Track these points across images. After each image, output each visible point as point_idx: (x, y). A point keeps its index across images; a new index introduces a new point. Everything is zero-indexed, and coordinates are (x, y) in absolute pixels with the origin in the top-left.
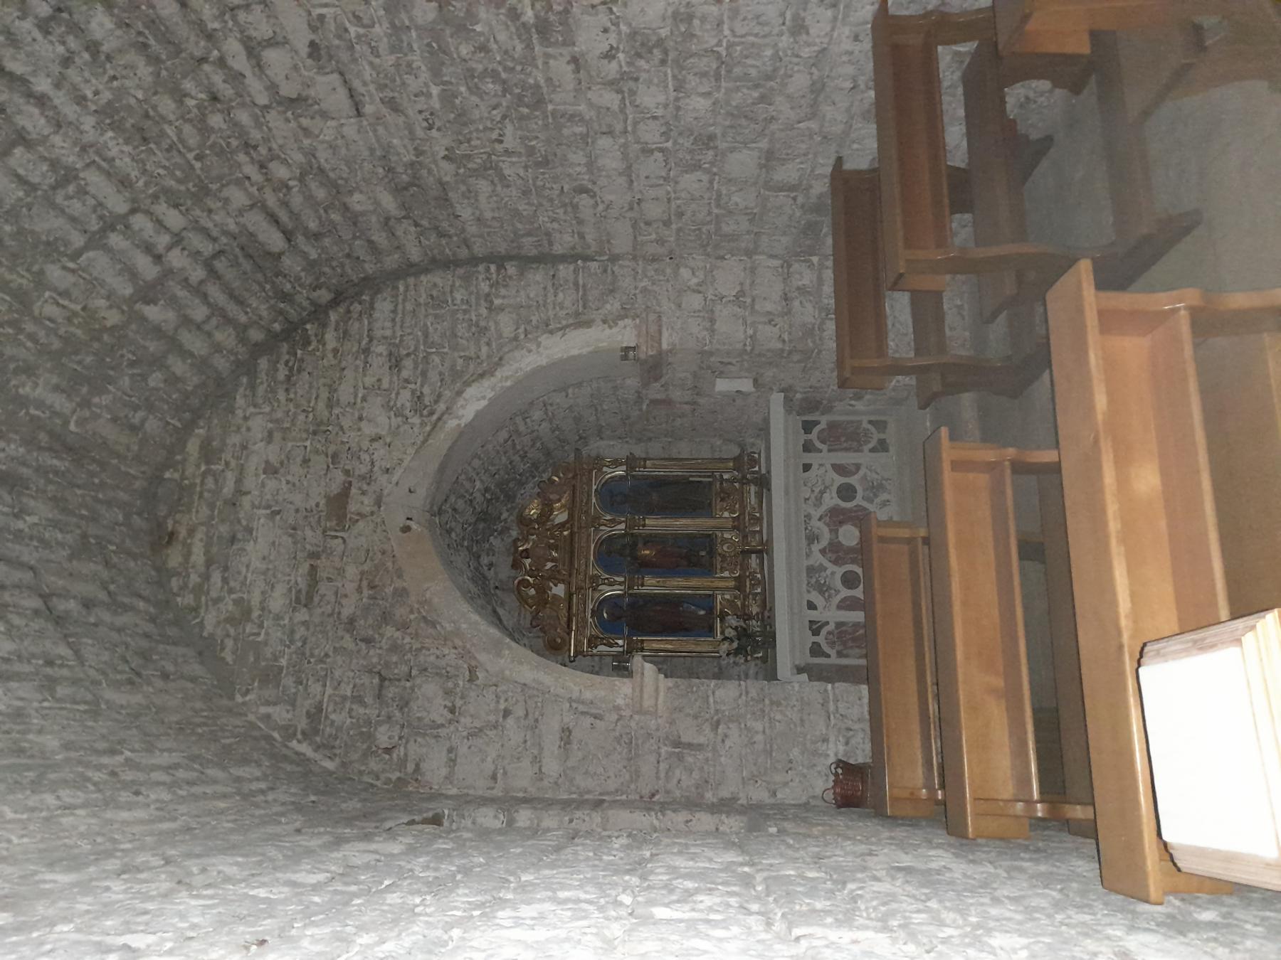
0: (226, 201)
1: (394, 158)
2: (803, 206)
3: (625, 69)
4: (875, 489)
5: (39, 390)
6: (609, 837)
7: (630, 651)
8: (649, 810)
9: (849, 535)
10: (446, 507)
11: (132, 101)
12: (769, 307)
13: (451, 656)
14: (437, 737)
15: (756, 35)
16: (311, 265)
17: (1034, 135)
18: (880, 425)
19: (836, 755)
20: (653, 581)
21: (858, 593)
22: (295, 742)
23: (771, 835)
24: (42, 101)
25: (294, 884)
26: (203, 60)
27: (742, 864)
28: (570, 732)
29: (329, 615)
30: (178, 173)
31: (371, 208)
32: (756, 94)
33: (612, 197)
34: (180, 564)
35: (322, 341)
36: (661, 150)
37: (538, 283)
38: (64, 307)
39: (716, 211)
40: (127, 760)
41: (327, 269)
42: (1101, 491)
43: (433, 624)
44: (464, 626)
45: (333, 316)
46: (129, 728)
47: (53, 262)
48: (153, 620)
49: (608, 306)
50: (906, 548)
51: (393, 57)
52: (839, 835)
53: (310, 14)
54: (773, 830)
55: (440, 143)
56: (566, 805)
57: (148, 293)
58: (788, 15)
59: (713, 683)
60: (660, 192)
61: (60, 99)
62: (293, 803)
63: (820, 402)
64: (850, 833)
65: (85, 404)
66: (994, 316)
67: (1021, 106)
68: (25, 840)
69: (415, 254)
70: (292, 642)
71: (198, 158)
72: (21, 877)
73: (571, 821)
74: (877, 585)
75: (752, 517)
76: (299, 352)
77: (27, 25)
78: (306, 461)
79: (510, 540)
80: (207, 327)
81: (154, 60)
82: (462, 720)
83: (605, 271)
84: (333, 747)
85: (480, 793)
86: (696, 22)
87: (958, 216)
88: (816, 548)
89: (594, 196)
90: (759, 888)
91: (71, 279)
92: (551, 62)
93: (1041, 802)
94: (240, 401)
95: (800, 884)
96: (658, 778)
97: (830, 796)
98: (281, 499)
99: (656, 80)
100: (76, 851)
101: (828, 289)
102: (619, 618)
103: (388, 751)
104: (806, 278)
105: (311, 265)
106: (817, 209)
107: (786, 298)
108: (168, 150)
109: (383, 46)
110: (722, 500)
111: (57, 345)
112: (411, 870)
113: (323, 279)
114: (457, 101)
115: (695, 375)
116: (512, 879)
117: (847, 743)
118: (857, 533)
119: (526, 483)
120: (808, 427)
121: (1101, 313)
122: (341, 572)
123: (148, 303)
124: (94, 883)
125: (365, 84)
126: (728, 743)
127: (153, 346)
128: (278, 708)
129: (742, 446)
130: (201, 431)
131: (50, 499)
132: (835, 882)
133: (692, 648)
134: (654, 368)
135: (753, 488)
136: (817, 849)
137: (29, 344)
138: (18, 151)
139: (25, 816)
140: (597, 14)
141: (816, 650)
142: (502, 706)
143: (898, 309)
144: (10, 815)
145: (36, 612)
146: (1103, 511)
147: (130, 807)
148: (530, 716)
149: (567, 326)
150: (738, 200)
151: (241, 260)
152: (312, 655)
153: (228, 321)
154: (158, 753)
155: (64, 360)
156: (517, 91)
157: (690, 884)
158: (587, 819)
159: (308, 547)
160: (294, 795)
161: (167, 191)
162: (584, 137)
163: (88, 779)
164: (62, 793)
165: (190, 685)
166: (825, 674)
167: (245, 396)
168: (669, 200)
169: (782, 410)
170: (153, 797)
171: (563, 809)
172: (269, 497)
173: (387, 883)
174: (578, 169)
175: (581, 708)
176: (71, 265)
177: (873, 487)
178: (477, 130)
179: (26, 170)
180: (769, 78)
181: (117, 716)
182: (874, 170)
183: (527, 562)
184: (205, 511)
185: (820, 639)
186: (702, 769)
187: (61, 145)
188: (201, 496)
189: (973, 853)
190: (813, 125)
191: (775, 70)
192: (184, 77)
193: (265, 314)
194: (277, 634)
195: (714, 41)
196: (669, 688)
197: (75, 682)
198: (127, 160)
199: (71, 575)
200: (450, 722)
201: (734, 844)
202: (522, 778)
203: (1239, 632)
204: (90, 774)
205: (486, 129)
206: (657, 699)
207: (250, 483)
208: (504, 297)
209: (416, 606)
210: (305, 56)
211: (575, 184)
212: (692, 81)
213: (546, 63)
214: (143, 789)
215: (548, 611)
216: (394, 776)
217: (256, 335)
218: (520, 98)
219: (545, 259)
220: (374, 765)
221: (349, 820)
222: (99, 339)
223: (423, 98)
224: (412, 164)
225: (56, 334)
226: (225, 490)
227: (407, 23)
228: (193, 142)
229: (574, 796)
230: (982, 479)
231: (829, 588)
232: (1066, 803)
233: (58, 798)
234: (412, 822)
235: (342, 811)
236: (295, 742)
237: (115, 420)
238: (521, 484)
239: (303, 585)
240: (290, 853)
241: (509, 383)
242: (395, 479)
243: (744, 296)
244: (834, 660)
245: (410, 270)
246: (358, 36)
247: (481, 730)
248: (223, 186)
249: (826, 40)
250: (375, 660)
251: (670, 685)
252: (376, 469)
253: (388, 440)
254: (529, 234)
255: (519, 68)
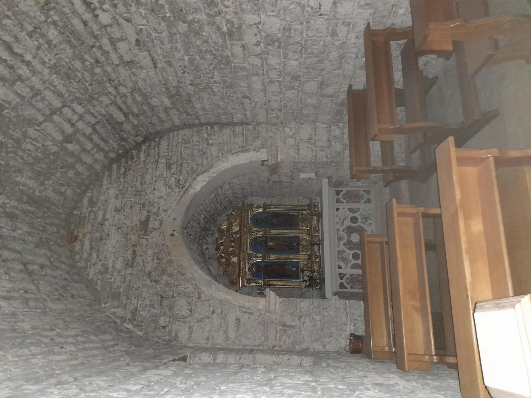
0: (101, 102)
1: (169, 84)
2: (336, 103)
3: (264, 50)
4: (366, 218)
5: (23, 179)
6: (257, 368)
7: (265, 285)
8: (273, 354)
9: (355, 238)
10: (189, 225)
11: (64, 63)
12: (322, 144)
13: (190, 287)
14: (184, 322)
15: (317, 37)
16: (135, 127)
17: (430, 76)
18: (368, 192)
19: (350, 331)
20: (274, 256)
21: (359, 262)
22: (126, 324)
23: (324, 367)
24: (28, 64)
25: (128, 391)
26: (93, 47)
27: (312, 382)
28: (240, 320)
29: (141, 271)
30: (82, 91)
31: (160, 104)
32: (316, 60)
33: (257, 100)
34: (80, 249)
35: (139, 158)
36: (278, 81)
37: (227, 134)
38: (35, 145)
39: (300, 105)
40: (57, 333)
41: (141, 128)
42: (458, 231)
43: (183, 274)
44: (196, 275)
45: (144, 147)
46: (57, 319)
47: (30, 127)
48: (68, 273)
49: (256, 144)
50: (378, 245)
51: (170, 45)
52: (352, 367)
53: (136, 28)
54: (324, 365)
55: (188, 78)
56: (239, 352)
57: (68, 139)
58: (330, 29)
59: (299, 299)
60: (278, 98)
61: (36, 63)
62: (126, 351)
63: (343, 182)
64: (356, 366)
65: (43, 184)
66: (414, 151)
67: (425, 64)
68: (17, 370)
69: (177, 122)
70: (125, 282)
71: (90, 85)
72: (17, 387)
73: (240, 359)
74: (367, 256)
75: (315, 230)
76: (129, 162)
77: (23, 34)
78: (132, 207)
79: (215, 238)
80: (92, 152)
81: (73, 47)
82: (195, 315)
83: (255, 129)
84: (142, 326)
85: (202, 346)
86: (292, 31)
87: (399, 108)
88: (341, 243)
89: (251, 99)
90: (319, 393)
91: (37, 133)
92: (234, 47)
93: (436, 355)
94: (105, 182)
95: (336, 392)
96: (276, 339)
97: (348, 348)
98: (121, 222)
99: (276, 54)
100: (38, 375)
101: (346, 136)
102: (260, 271)
103: (164, 327)
104: (337, 132)
105: (135, 127)
106: (342, 104)
107: (329, 140)
108: (78, 82)
109: (166, 41)
110: (303, 222)
111: (31, 160)
112: (175, 384)
113: (140, 132)
114: (195, 62)
115: (291, 171)
116: (217, 388)
117: (355, 325)
118: (359, 237)
119: (222, 214)
120: (338, 193)
121: (458, 159)
122: (146, 252)
123: (68, 143)
124: (46, 390)
125: (158, 56)
126: (305, 325)
127: (70, 160)
128: (119, 309)
129: (310, 199)
130: (89, 194)
131: (27, 223)
132: (350, 391)
133: (290, 284)
134: (274, 169)
135: (315, 218)
136: (342, 374)
137: (20, 160)
138: (18, 83)
139: (17, 359)
140: (252, 28)
141: (342, 286)
142: (212, 309)
143: (375, 147)
144: (10, 359)
145: (21, 271)
146: (460, 240)
147: (59, 354)
148: (223, 313)
149: (238, 152)
150: (309, 101)
151: (107, 125)
152: (133, 287)
153: (102, 150)
154: (70, 330)
155: (34, 166)
156: (219, 58)
157: (291, 392)
158: (247, 358)
159: (132, 242)
160: (126, 347)
161: (77, 98)
162: (247, 77)
163: (42, 342)
164: (31, 348)
165: (83, 300)
166: (345, 295)
167: (107, 180)
168: (281, 101)
169: (327, 186)
170: (68, 349)
171: (237, 353)
172: (116, 221)
173: (166, 390)
174: (244, 89)
175: (245, 310)
176: (38, 128)
177: (365, 218)
178: (203, 73)
179: (21, 91)
180: (322, 53)
181: (54, 314)
182: (364, 90)
183: (222, 248)
184: (90, 228)
185: (343, 281)
186: (294, 336)
187: (35, 81)
188: (88, 221)
189: (407, 376)
190: (340, 71)
191: (324, 50)
192: (85, 54)
193: (115, 146)
194: (119, 279)
195: (299, 39)
196: (281, 302)
197: (36, 300)
198: (61, 86)
199: (35, 255)
200: (190, 316)
201: (308, 371)
202: (219, 340)
203: (514, 303)
204: (43, 340)
205: (207, 73)
206: (276, 307)
207: (108, 216)
208: (213, 140)
209: (176, 267)
210: (134, 45)
211: (243, 95)
212: (291, 55)
213: (231, 47)
214: (64, 346)
215: (230, 268)
216: (167, 338)
217: (112, 155)
218: (221, 61)
219: (231, 124)
220: (158, 333)
221: (148, 359)
222: (49, 158)
223: (181, 61)
224: (177, 87)
225: (31, 156)
226: (98, 219)
227: (175, 31)
228: (88, 79)
229: (241, 347)
230: (410, 220)
231: (347, 260)
232: (446, 355)
233: (30, 351)
234: (174, 360)
235: (145, 354)
236: (126, 324)
237: (54, 190)
238: (220, 215)
239: (129, 257)
240: (125, 375)
241: (215, 175)
242: (168, 214)
243: (312, 139)
244: (349, 290)
245: (174, 128)
246: (156, 37)
247: (203, 319)
248: (100, 96)
249: (345, 38)
250: (159, 289)
251: (281, 300)
252: (160, 210)
253: (165, 198)
254: (224, 114)
255: (220, 49)
